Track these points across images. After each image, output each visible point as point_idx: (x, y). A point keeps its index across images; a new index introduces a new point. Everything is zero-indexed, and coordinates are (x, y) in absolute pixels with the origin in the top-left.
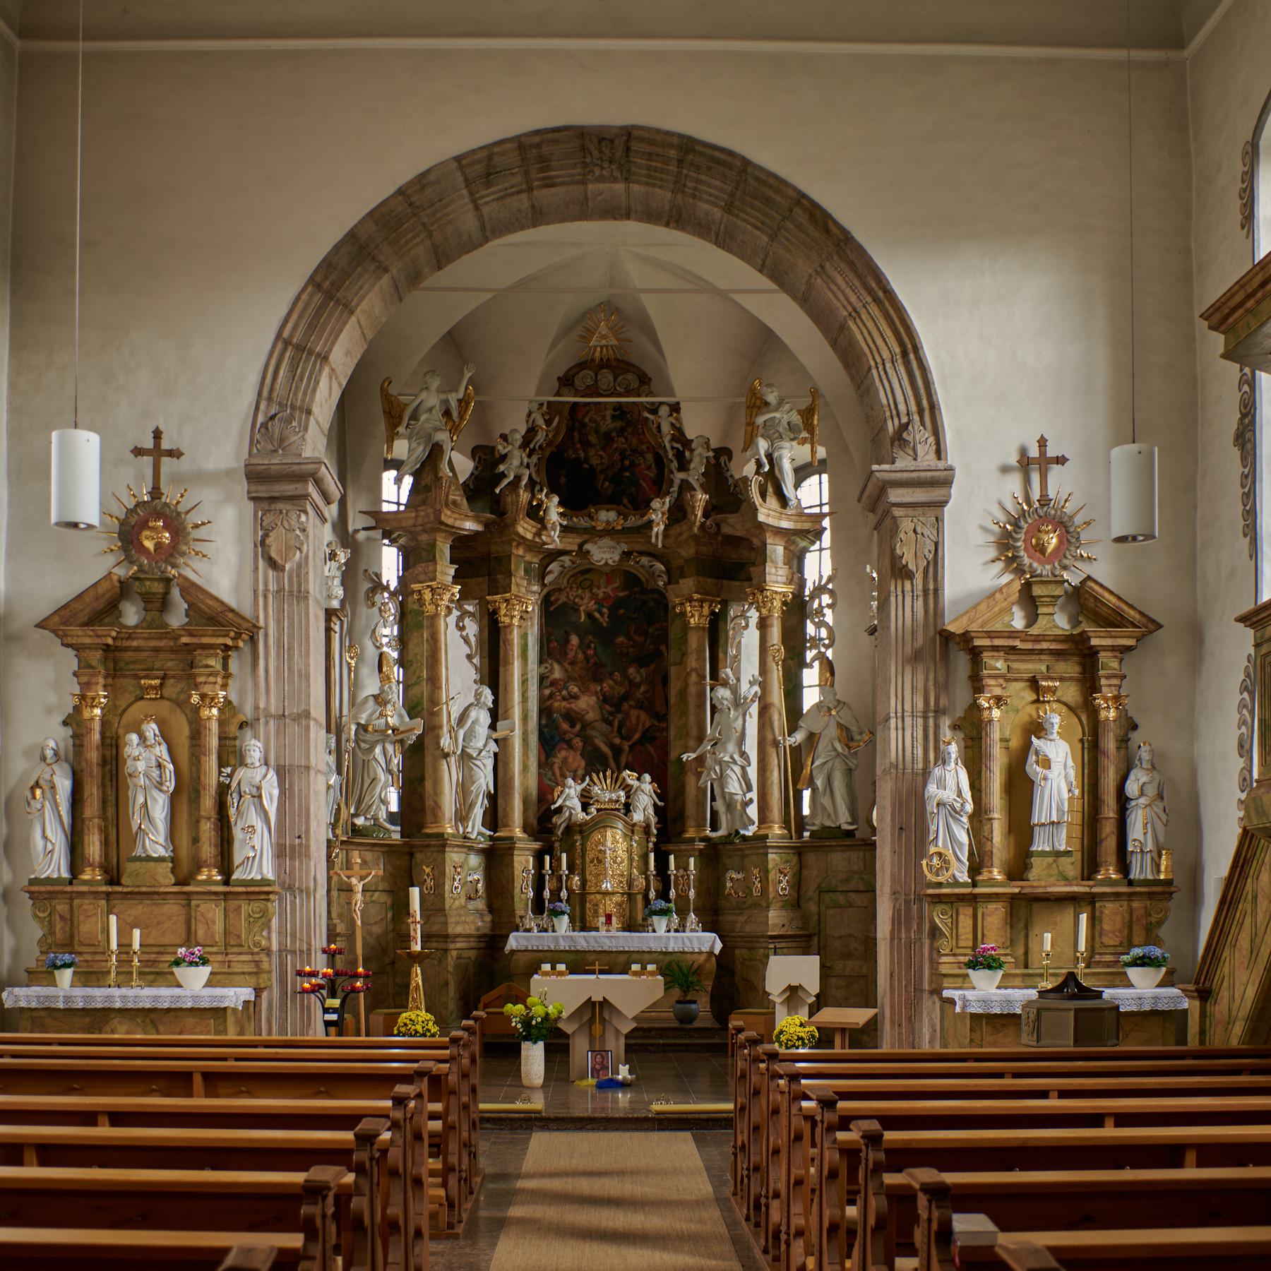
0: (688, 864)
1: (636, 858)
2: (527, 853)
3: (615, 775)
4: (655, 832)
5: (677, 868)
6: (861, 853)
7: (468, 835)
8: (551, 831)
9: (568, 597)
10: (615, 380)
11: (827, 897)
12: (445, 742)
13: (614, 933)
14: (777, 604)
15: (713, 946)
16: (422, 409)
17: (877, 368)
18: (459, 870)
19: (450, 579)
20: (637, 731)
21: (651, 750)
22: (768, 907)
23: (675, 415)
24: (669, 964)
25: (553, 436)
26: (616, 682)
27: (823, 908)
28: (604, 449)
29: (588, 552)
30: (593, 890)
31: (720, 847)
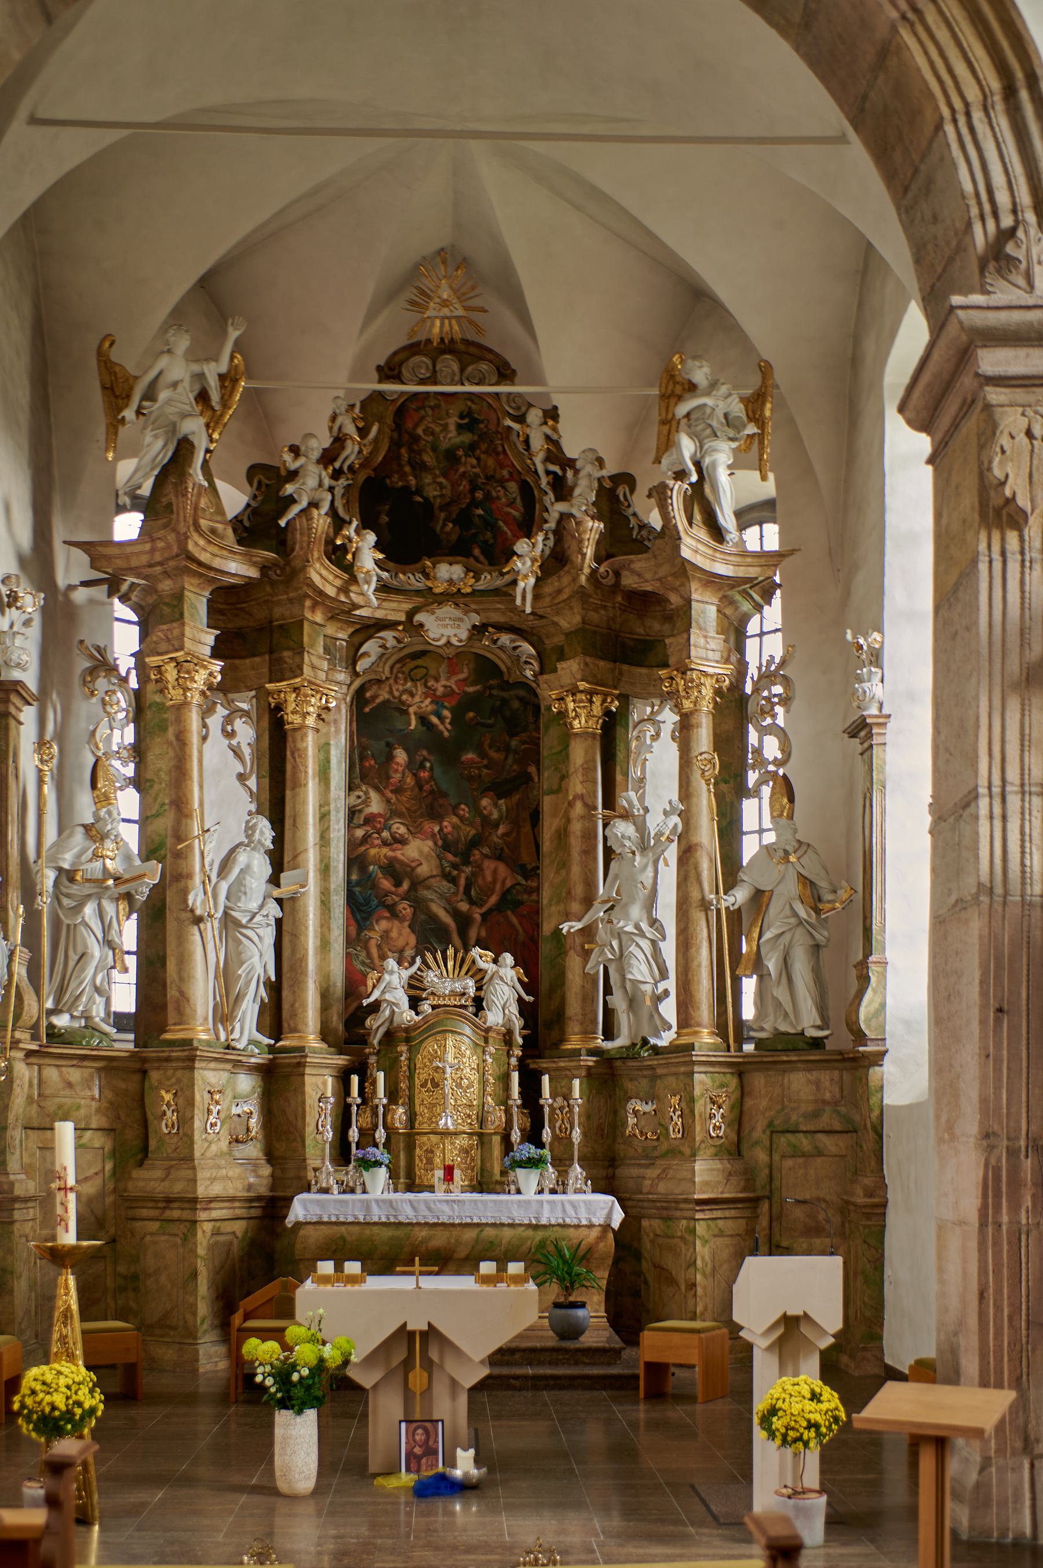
0: (570, 1089)
1: (492, 1080)
2: (326, 1071)
3: (460, 955)
4: (520, 1041)
5: (553, 1096)
6: (836, 1073)
7: (233, 1044)
8: (364, 1041)
9: (391, 692)
10: (462, 370)
11: (783, 1141)
12: (196, 899)
13: (457, 1195)
14: (707, 692)
15: (609, 1216)
16: (162, 381)
17: (955, 121)
18: (217, 1097)
19: (207, 651)
20: (493, 891)
21: (514, 920)
22: (694, 1155)
23: (550, 423)
24: (542, 1244)
25: (371, 453)
26: (462, 819)
27: (776, 1157)
28: (445, 475)
29: (421, 625)
30: (426, 1129)
31: (618, 1063)
